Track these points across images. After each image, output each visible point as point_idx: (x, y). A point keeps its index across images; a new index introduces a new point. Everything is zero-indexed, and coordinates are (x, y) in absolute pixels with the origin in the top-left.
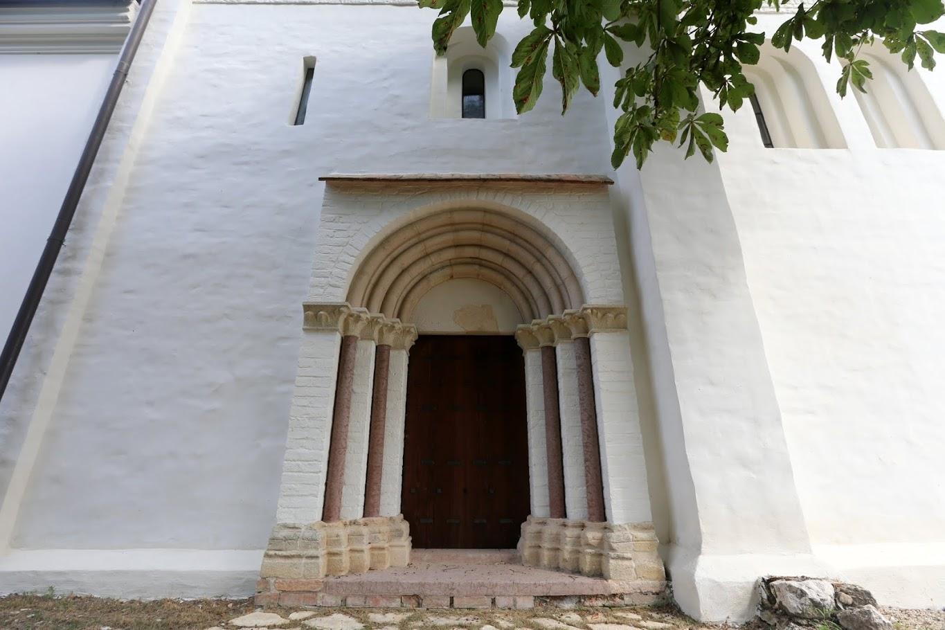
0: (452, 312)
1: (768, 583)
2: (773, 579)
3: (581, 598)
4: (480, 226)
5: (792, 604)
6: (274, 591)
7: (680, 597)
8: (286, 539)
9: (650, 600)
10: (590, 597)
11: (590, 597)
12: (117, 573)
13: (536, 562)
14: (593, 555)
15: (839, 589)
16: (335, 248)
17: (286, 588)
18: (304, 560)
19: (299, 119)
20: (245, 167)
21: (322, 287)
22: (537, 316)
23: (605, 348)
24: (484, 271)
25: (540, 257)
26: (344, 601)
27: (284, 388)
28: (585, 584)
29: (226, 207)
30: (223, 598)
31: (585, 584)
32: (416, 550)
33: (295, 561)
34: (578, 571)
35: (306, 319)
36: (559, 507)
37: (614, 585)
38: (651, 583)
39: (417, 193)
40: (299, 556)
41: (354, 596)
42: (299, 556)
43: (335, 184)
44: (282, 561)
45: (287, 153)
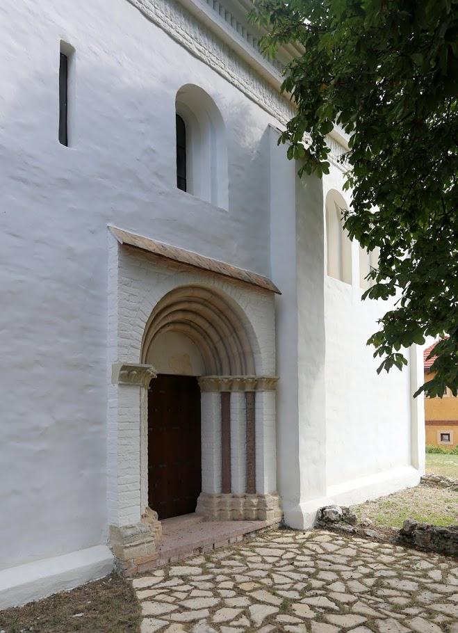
0: (177, 361)
1: (323, 510)
2: (324, 509)
3: (256, 531)
4: (202, 301)
5: (334, 517)
6: (134, 566)
7: (288, 522)
8: (133, 535)
9: (278, 525)
10: (260, 530)
11: (260, 530)
12: (8, 590)
13: (221, 518)
14: (256, 510)
15: (343, 509)
16: (131, 312)
17: (139, 562)
18: (146, 545)
19: (64, 138)
20: (25, 187)
21: (127, 348)
22: (226, 368)
23: (264, 400)
24: (194, 332)
25: (234, 330)
26: (169, 561)
27: (94, 429)
28: (258, 524)
29: (14, 235)
30: (91, 581)
31: (258, 524)
32: (167, 521)
33: (141, 546)
34: (246, 519)
35: (121, 376)
36: (226, 486)
37: (268, 522)
38: (278, 519)
39: (180, 270)
40: (143, 543)
41: (173, 556)
42: (143, 543)
43: (130, 251)
44: (135, 548)
45: (66, 183)
